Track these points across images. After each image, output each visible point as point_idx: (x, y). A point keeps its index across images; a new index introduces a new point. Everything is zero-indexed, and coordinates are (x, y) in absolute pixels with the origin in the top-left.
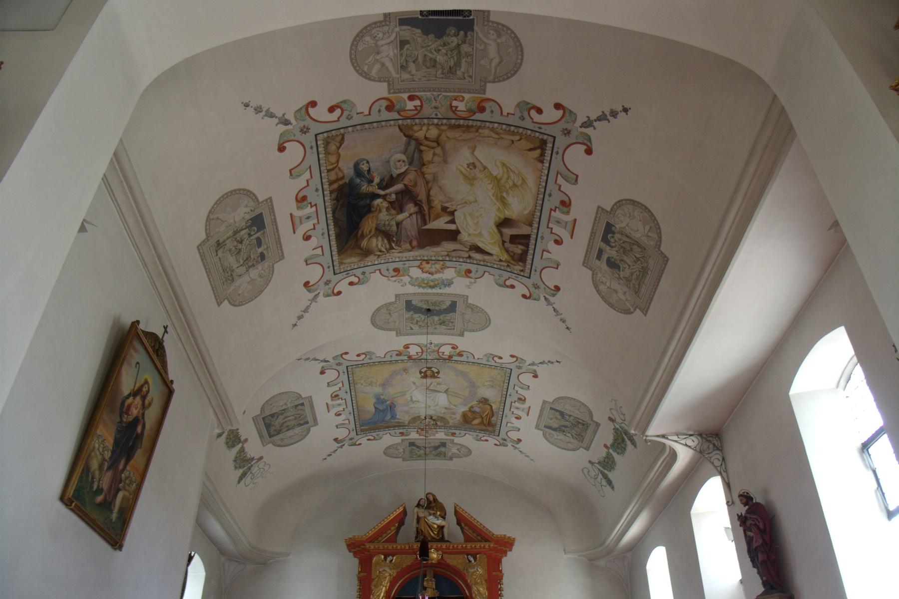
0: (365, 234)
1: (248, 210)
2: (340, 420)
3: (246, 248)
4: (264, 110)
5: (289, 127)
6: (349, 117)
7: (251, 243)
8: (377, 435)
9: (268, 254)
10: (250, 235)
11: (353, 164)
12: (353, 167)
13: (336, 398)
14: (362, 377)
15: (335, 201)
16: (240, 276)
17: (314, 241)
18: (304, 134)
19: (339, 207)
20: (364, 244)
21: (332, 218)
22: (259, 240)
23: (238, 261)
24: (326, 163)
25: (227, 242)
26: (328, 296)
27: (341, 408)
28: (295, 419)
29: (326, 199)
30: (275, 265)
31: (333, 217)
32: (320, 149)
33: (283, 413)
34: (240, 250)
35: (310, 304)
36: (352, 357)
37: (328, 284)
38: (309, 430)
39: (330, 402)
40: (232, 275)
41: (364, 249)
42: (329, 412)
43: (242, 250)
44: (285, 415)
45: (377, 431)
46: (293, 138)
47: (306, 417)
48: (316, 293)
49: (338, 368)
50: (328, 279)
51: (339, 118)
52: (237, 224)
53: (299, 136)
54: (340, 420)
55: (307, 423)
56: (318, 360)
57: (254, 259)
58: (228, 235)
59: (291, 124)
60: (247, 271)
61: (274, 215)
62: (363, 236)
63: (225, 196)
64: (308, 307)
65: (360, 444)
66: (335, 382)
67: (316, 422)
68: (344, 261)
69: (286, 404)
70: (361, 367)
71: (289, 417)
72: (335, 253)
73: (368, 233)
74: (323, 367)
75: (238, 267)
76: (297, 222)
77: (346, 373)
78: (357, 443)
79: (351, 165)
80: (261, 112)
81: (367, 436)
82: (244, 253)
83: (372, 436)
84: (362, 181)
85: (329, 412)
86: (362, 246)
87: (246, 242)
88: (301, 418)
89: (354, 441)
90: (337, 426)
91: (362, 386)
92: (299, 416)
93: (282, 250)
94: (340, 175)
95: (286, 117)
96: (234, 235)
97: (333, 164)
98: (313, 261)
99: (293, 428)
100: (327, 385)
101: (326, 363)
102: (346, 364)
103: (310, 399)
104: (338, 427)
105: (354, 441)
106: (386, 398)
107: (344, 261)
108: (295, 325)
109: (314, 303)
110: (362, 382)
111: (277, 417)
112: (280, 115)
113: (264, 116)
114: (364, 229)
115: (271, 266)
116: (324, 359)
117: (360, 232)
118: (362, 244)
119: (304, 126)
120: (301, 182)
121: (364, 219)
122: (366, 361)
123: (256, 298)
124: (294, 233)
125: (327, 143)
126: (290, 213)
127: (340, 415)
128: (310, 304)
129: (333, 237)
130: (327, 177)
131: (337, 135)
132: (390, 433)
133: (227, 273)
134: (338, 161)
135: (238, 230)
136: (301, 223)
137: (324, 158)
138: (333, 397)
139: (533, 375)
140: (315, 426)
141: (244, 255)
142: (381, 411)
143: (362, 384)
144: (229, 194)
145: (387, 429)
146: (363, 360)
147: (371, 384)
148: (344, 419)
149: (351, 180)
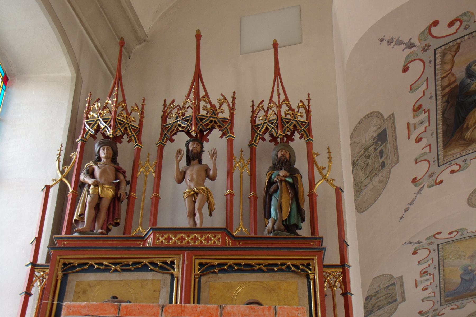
0: (469, 126)
1: (375, 128)
2: (426, 294)
3: (372, 161)
4: (395, 40)
5: (414, 49)
6: (467, 27)
7: (376, 156)
8: (461, 304)
9: (387, 161)
10: (375, 149)
11: (465, 68)
12: (465, 70)
13: (425, 274)
14: (451, 252)
15: (445, 103)
16: (366, 186)
17: (424, 142)
18: (425, 52)
19: (448, 108)
20: (468, 135)
21: (441, 118)
22: (381, 152)
23: (365, 174)
24: (441, 72)
25: (359, 160)
26: (431, 186)
27: (428, 283)
28: (385, 299)
29: (438, 103)
30: (392, 170)
31: (442, 117)
32: (437, 62)
33: (376, 295)
34: (368, 164)
35: (416, 197)
36: (445, 235)
37: (432, 176)
38: (397, 307)
39: (419, 279)
40: (360, 187)
41: (467, 140)
42: (416, 288)
43: (369, 163)
44: (377, 296)
45: (461, 300)
46: (416, 58)
47: (396, 295)
48: (422, 186)
49: (430, 247)
50: (433, 172)
51: (457, 30)
52: (367, 143)
53: (422, 55)
54: (426, 294)
55: (396, 300)
56: (413, 243)
57: (377, 168)
58: (360, 154)
59: (415, 46)
60: (371, 180)
61: (395, 128)
62: (467, 129)
63: (361, 122)
64: (414, 200)
65: (443, 314)
66: (425, 260)
67: (404, 299)
68: (448, 154)
69: (379, 286)
70: (452, 243)
71: (381, 297)
72: (441, 148)
73: (472, 125)
74: (415, 249)
75: (365, 179)
76: (412, 128)
77: (437, 251)
78: (440, 314)
79: (464, 69)
80: (392, 43)
81: (450, 306)
82: (370, 166)
83: (455, 305)
84: (472, 80)
85: (416, 288)
86: (465, 137)
87: (372, 156)
88: (391, 297)
89: (437, 312)
90: (423, 301)
91: (451, 261)
92: (389, 295)
93: (398, 155)
94: (453, 79)
95: (412, 41)
96: (364, 153)
97: (447, 71)
98: (421, 159)
99: (383, 307)
100: (418, 263)
101: (419, 245)
102: (437, 242)
103: (401, 279)
104: (424, 300)
105: (437, 312)
106: (473, 269)
107: (448, 154)
108: (402, 217)
109: (419, 195)
110: (451, 256)
111: (371, 299)
112: (406, 41)
113: (395, 45)
114: (470, 122)
115: (389, 171)
116: (418, 241)
117: (465, 126)
118: (467, 135)
119: (426, 45)
120: (419, 93)
121: (470, 114)
122: (458, 237)
123: (375, 201)
124: (409, 138)
125: (444, 54)
126: (407, 122)
127: (426, 289)
128: (416, 197)
129: (440, 135)
130: (441, 84)
131: (454, 45)
132: (474, 301)
133: (358, 186)
134: (451, 69)
135: (368, 147)
136: (415, 129)
137: (440, 68)
138: (422, 274)
139: (423, 312)
140: (402, 302)
141: (370, 168)
142: (467, 281)
143: (451, 259)
144: (363, 119)
145: (471, 298)
146: (455, 236)
147: (460, 257)
148: (430, 292)
149: (462, 82)
